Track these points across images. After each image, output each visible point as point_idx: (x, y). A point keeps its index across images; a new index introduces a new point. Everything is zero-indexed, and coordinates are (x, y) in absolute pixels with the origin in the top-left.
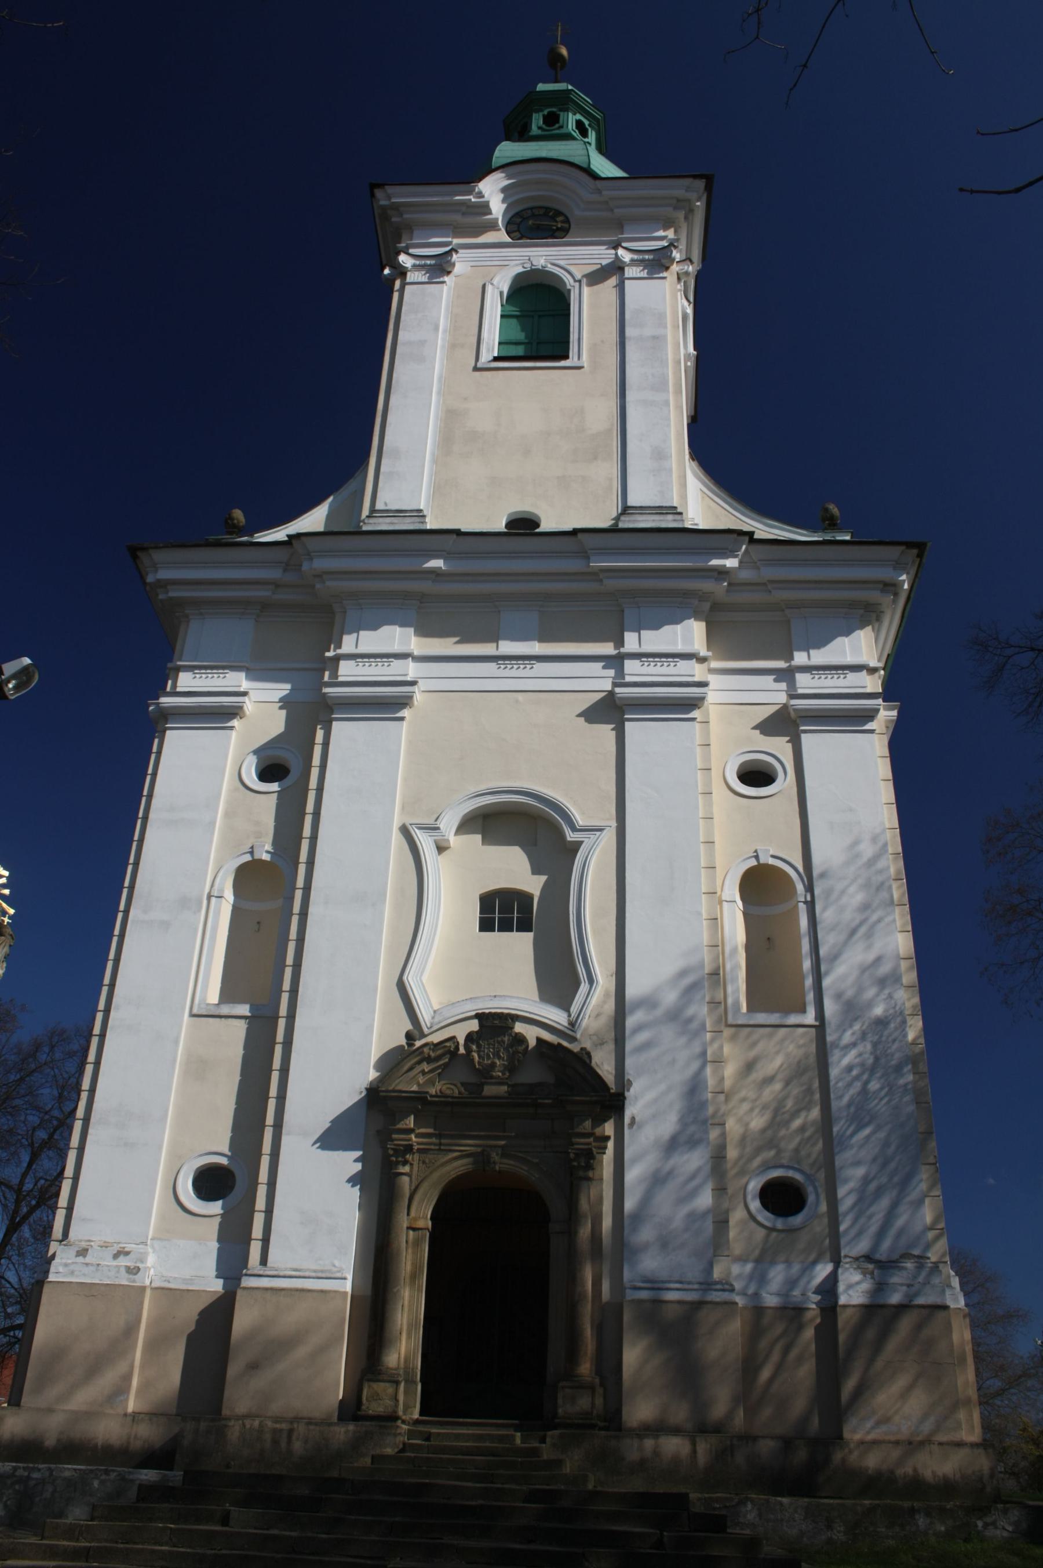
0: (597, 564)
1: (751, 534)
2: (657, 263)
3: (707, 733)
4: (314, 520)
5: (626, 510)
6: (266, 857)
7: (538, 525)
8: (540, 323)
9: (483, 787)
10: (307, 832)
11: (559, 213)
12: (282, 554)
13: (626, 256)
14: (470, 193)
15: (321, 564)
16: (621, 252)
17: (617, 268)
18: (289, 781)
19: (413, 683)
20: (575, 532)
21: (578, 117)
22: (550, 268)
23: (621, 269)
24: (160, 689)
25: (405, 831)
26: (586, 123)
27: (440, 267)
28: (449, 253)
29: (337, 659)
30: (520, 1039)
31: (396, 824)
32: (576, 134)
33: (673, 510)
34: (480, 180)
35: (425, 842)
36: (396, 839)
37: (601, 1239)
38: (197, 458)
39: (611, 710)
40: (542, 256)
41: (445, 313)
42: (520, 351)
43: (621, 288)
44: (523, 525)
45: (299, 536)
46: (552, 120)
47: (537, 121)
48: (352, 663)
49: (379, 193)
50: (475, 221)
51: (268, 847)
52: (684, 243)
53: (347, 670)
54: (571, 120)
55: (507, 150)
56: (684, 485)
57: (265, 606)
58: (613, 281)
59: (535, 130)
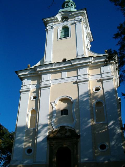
0: (73, 64)
1: (93, 56)
2: (80, 21)
3: (89, 85)
4: (38, 64)
5: (77, 56)
6: (34, 109)
7: (66, 60)
8: (66, 31)
9: (62, 96)
10: (39, 105)
11: (67, 17)
12: (32, 70)
13: (75, 21)
14: (55, 17)
15: (38, 70)
16: (75, 21)
17: (75, 23)
18: (36, 99)
19: (51, 84)
20: (70, 60)
21: (71, 4)
22: (66, 25)
23: (75, 23)
24: (20, 89)
25: (51, 103)
26: (72, 4)
27: (52, 27)
28: (53, 26)
29: (22, 86)
30: (66, 129)
31: (50, 102)
32: (71, 6)
33: (84, 55)
34: (56, 15)
35: (53, 104)
36: (50, 104)
37: (44, 138)
38: (28, 55)
39: (76, 83)
40: (65, 24)
41: (54, 32)
42: (63, 37)
43: (75, 25)
44: (64, 60)
45: (35, 67)
46: (67, 5)
47: (65, 5)
48: (43, 82)
49: (43, 20)
50: (56, 20)
51: (34, 108)
52: (84, 17)
53: (43, 83)
54: (70, 4)
55: (61, 10)
56: (85, 51)
57: (33, 76)
58: (74, 25)
59: (65, 7)
